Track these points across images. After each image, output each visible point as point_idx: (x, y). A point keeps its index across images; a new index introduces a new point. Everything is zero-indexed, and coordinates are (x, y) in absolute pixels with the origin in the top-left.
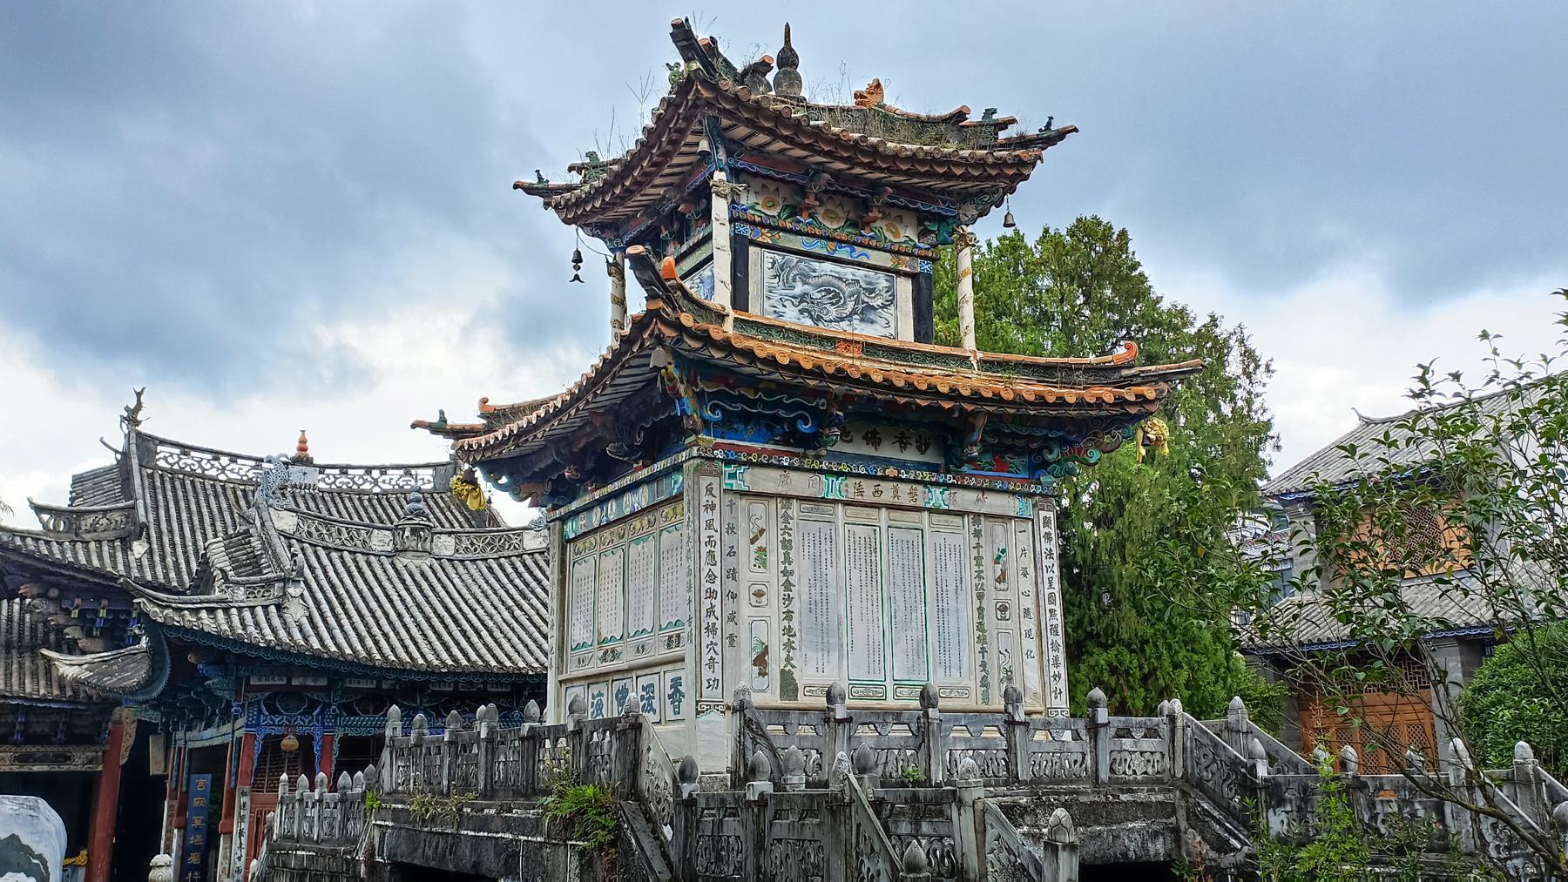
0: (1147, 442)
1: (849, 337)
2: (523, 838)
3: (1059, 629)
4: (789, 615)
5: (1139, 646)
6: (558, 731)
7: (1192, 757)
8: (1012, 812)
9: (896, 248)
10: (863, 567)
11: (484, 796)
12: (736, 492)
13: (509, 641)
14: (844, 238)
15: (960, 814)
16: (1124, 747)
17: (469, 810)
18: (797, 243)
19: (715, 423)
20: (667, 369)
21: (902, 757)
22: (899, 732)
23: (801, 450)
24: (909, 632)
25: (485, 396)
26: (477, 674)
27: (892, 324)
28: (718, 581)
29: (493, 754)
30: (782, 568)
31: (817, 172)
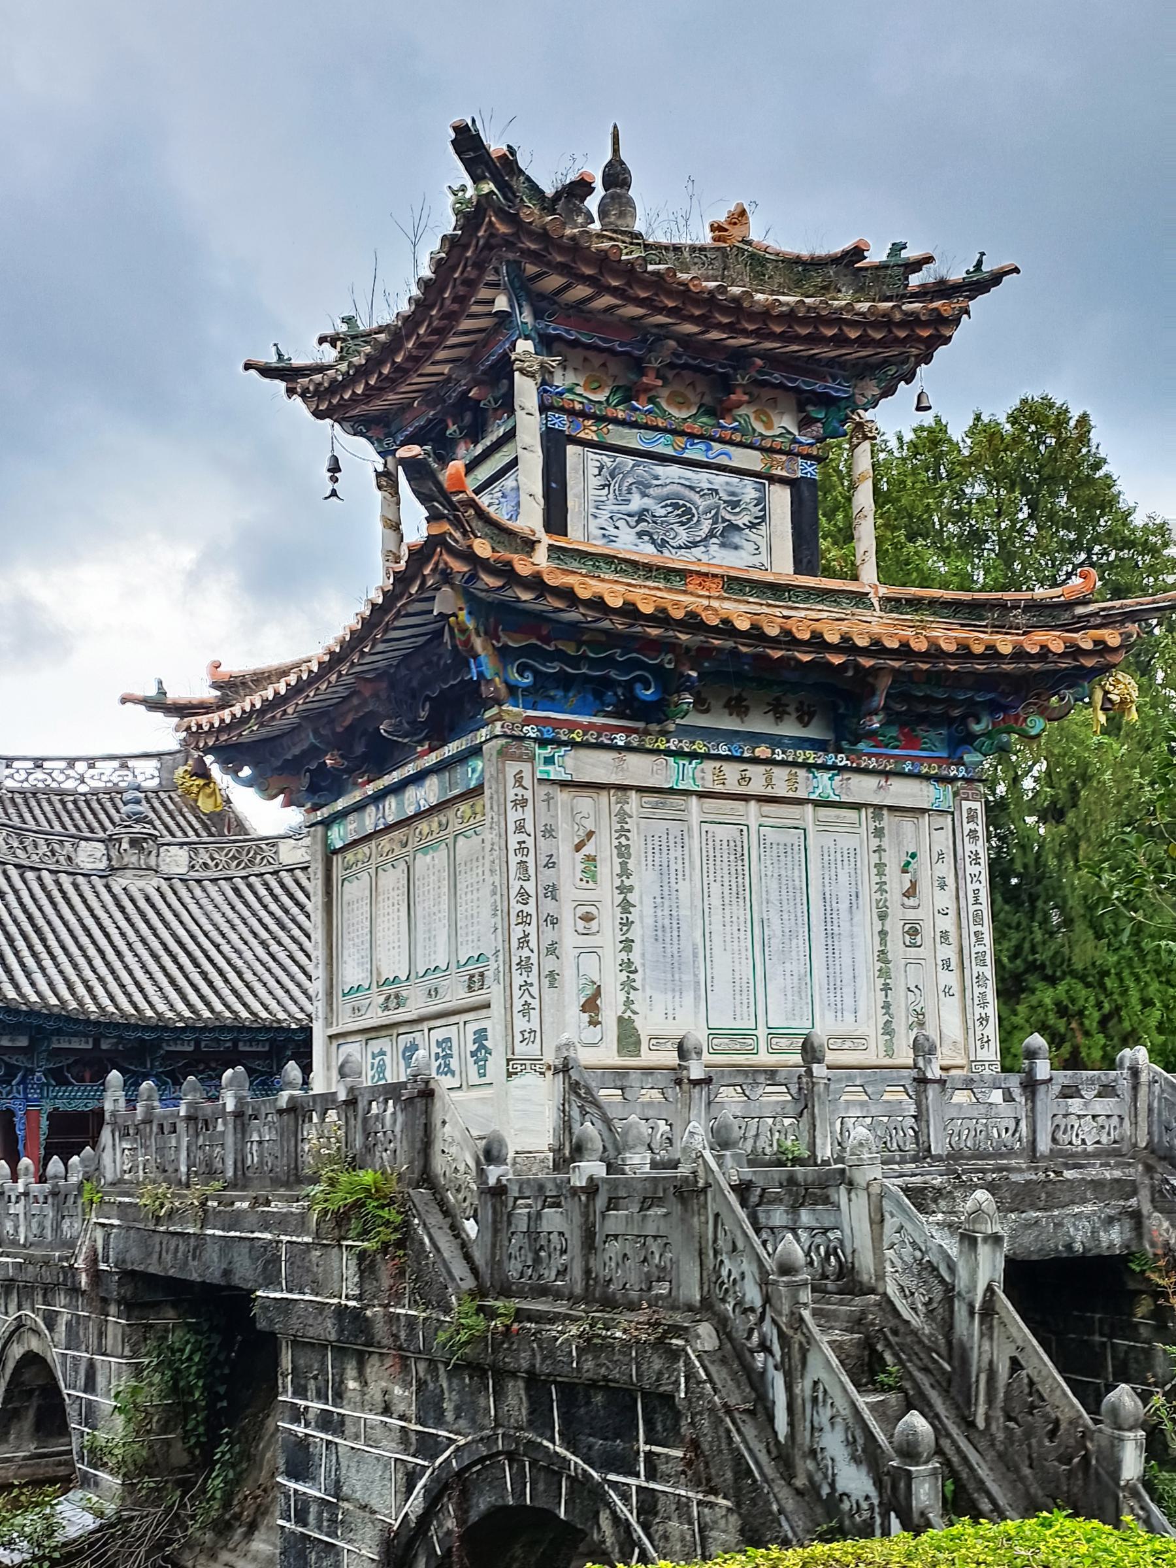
0: (1107, 705)
1: (704, 569)
2: (285, 1238)
3: (988, 958)
4: (627, 945)
5: (1096, 978)
6: (327, 1101)
7: (1160, 1121)
8: (920, 1197)
9: (767, 444)
10: (726, 879)
11: (232, 1185)
12: (553, 782)
13: (265, 985)
14: (697, 430)
15: (850, 1200)
16: (1071, 1110)
17: (215, 1204)
18: (633, 439)
19: (524, 690)
20: (457, 617)
21: (778, 1127)
22: (775, 1096)
23: (640, 725)
24: (787, 965)
25: (215, 657)
26: (224, 1029)
27: (763, 549)
28: (532, 901)
29: (244, 1132)
30: (618, 883)
31: (659, 339)
